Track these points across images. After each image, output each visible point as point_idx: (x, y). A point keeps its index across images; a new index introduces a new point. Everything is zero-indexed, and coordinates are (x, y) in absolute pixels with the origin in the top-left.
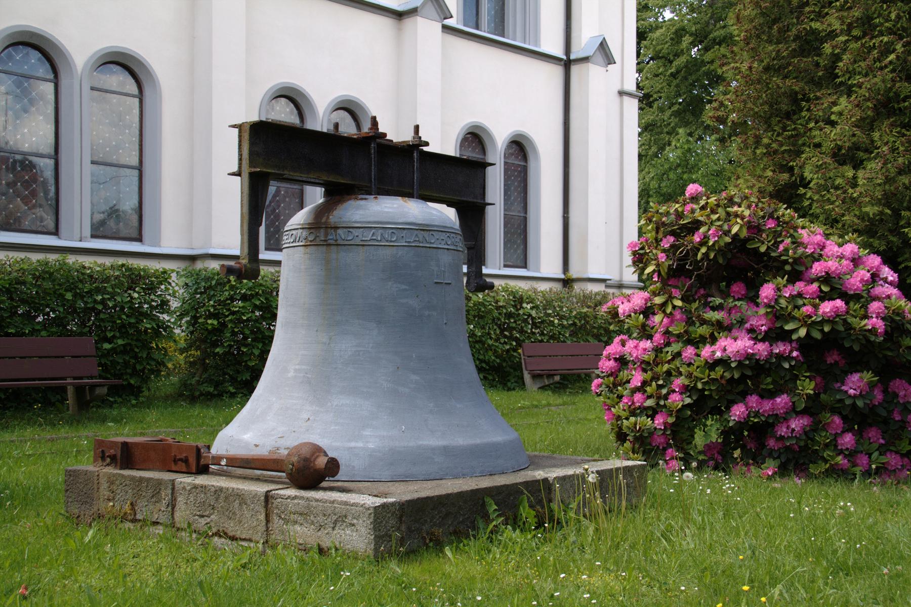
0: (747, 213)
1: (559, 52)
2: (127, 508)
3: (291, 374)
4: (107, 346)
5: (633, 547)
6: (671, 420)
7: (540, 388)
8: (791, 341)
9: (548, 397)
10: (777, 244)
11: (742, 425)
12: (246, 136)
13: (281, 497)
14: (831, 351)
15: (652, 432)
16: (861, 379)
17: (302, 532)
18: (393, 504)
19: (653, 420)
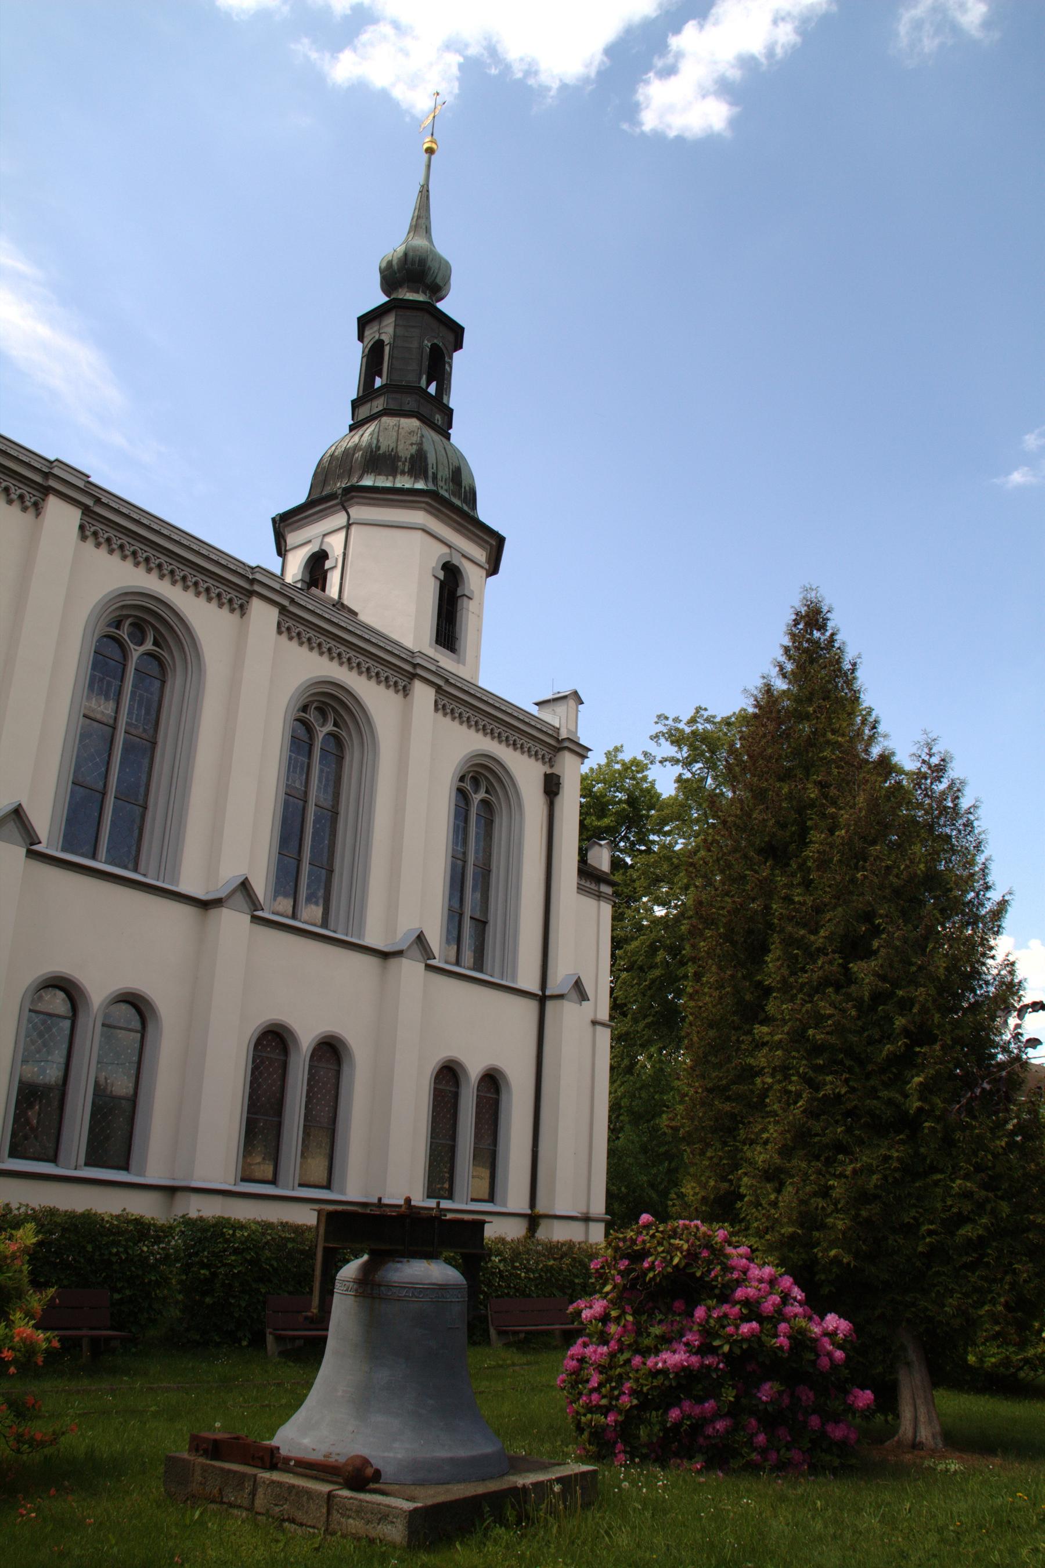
0: (686, 1247)
1: (534, 987)
2: (216, 1491)
3: (340, 1394)
4: (117, 1296)
5: (584, 1543)
6: (620, 1418)
7: (505, 1344)
8: (718, 1355)
9: (513, 1356)
10: (709, 1271)
11: (677, 1425)
12: (323, 1219)
13: (341, 1497)
14: (749, 1363)
15: (605, 1428)
16: (771, 1388)
17: (354, 1525)
18: (421, 1508)
19: (606, 1418)
